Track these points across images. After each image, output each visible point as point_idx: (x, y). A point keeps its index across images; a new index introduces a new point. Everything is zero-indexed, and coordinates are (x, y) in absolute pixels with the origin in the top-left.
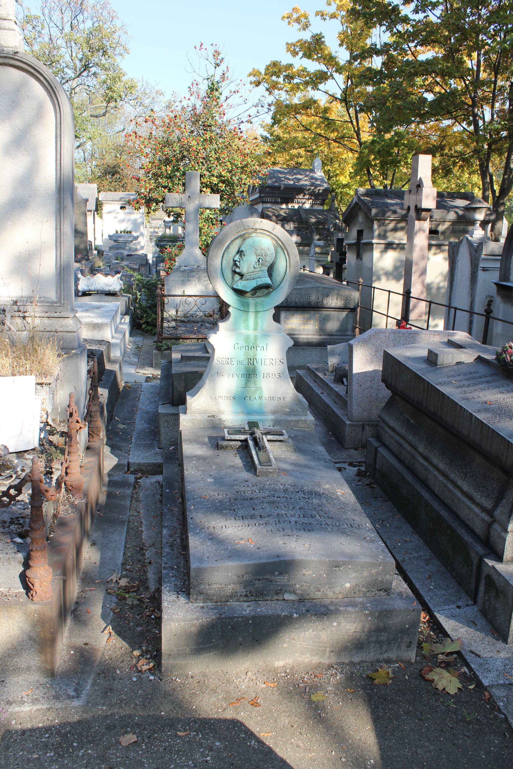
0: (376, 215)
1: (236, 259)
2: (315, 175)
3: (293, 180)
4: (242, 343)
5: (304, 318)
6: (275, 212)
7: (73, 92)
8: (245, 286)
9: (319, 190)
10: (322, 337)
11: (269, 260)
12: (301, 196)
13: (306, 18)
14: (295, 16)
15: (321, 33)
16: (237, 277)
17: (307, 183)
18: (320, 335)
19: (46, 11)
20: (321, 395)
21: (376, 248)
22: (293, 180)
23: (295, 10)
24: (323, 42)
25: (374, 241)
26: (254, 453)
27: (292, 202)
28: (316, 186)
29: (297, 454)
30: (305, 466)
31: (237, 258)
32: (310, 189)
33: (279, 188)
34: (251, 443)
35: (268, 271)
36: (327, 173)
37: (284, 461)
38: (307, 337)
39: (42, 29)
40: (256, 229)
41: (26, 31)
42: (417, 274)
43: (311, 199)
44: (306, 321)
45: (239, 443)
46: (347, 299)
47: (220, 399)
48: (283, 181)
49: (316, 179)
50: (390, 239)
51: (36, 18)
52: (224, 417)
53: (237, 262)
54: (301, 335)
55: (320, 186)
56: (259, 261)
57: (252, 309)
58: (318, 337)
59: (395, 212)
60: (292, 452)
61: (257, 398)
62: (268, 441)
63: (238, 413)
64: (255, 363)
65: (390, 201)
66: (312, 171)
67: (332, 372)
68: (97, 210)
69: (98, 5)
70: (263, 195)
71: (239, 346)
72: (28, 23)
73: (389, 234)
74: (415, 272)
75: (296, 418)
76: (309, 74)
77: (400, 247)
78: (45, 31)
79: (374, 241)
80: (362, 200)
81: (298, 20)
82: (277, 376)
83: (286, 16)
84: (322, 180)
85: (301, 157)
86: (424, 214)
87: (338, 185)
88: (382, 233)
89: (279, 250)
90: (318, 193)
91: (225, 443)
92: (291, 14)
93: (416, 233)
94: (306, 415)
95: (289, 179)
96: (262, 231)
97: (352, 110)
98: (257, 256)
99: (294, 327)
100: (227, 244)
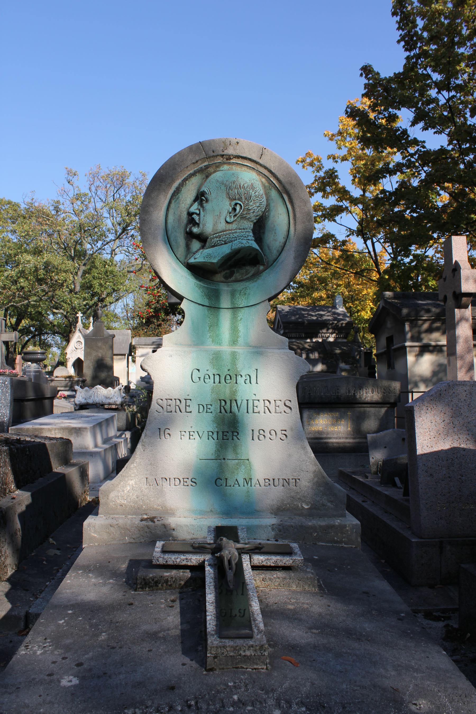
0: (408, 315)
1: (193, 209)
2: (337, 311)
3: (315, 316)
4: (207, 368)
5: (333, 418)
6: (300, 345)
7: (114, 253)
8: (209, 256)
9: (342, 324)
10: (357, 440)
11: (256, 208)
12: (324, 331)
13: (319, 161)
14: (308, 160)
15: (334, 168)
16: (196, 245)
17: (330, 318)
18: (354, 438)
19: (93, 189)
20: (363, 504)
21: (410, 352)
22: (315, 316)
23: (308, 154)
24: (336, 177)
25: (407, 344)
26: (210, 597)
27: (316, 337)
28: (339, 320)
29: (325, 601)
30: (349, 633)
31: (194, 208)
32: (333, 323)
33: (303, 323)
34: (209, 570)
35: (254, 231)
36: (349, 309)
37: (292, 616)
38: (337, 441)
39: (89, 202)
40: (229, 158)
41: (74, 204)
42: (464, 370)
43: (334, 333)
44: (336, 421)
45: (188, 574)
46: (387, 391)
47: (166, 484)
48: (306, 317)
49: (339, 314)
50: (425, 341)
51: (85, 195)
52: (172, 521)
53: (194, 216)
54: (330, 438)
55: (342, 320)
56: (234, 209)
57: (225, 302)
58: (351, 441)
59: (428, 311)
60: (314, 594)
61: (241, 481)
62: (254, 568)
63: (202, 513)
64: (235, 409)
65: (420, 302)
66: (334, 307)
67: (376, 473)
68: (130, 354)
69: (137, 181)
70: (287, 331)
71: (201, 375)
72: (78, 199)
73: (423, 335)
74: (461, 368)
75: (322, 523)
76: (325, 209)
77: (437, 349)
78: (91, 206)
79: (407, 344)
80: (389, 302)
81: (311, 164)
82: (280, 435)
83: (300, 160)
84: (344, 315)
85: (323, 300)
86: (464, 299)
87: (360, 320)
88: (416, 335)
89: (274, 193)
90: (342, 326)
91: (153, 574)
92: (305, 158)
93: (458, 323)
94: (344, 516)
95: (312, 316)
96: (240, 161)
97: (369, 242)
98: (231, 199)
99: (320, 428)
100: (176, 184)
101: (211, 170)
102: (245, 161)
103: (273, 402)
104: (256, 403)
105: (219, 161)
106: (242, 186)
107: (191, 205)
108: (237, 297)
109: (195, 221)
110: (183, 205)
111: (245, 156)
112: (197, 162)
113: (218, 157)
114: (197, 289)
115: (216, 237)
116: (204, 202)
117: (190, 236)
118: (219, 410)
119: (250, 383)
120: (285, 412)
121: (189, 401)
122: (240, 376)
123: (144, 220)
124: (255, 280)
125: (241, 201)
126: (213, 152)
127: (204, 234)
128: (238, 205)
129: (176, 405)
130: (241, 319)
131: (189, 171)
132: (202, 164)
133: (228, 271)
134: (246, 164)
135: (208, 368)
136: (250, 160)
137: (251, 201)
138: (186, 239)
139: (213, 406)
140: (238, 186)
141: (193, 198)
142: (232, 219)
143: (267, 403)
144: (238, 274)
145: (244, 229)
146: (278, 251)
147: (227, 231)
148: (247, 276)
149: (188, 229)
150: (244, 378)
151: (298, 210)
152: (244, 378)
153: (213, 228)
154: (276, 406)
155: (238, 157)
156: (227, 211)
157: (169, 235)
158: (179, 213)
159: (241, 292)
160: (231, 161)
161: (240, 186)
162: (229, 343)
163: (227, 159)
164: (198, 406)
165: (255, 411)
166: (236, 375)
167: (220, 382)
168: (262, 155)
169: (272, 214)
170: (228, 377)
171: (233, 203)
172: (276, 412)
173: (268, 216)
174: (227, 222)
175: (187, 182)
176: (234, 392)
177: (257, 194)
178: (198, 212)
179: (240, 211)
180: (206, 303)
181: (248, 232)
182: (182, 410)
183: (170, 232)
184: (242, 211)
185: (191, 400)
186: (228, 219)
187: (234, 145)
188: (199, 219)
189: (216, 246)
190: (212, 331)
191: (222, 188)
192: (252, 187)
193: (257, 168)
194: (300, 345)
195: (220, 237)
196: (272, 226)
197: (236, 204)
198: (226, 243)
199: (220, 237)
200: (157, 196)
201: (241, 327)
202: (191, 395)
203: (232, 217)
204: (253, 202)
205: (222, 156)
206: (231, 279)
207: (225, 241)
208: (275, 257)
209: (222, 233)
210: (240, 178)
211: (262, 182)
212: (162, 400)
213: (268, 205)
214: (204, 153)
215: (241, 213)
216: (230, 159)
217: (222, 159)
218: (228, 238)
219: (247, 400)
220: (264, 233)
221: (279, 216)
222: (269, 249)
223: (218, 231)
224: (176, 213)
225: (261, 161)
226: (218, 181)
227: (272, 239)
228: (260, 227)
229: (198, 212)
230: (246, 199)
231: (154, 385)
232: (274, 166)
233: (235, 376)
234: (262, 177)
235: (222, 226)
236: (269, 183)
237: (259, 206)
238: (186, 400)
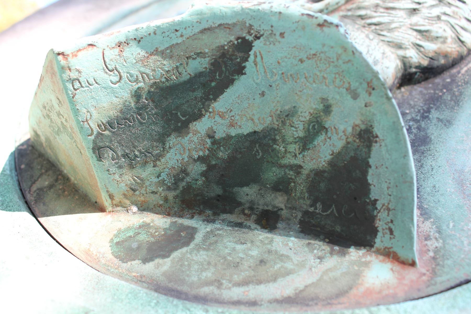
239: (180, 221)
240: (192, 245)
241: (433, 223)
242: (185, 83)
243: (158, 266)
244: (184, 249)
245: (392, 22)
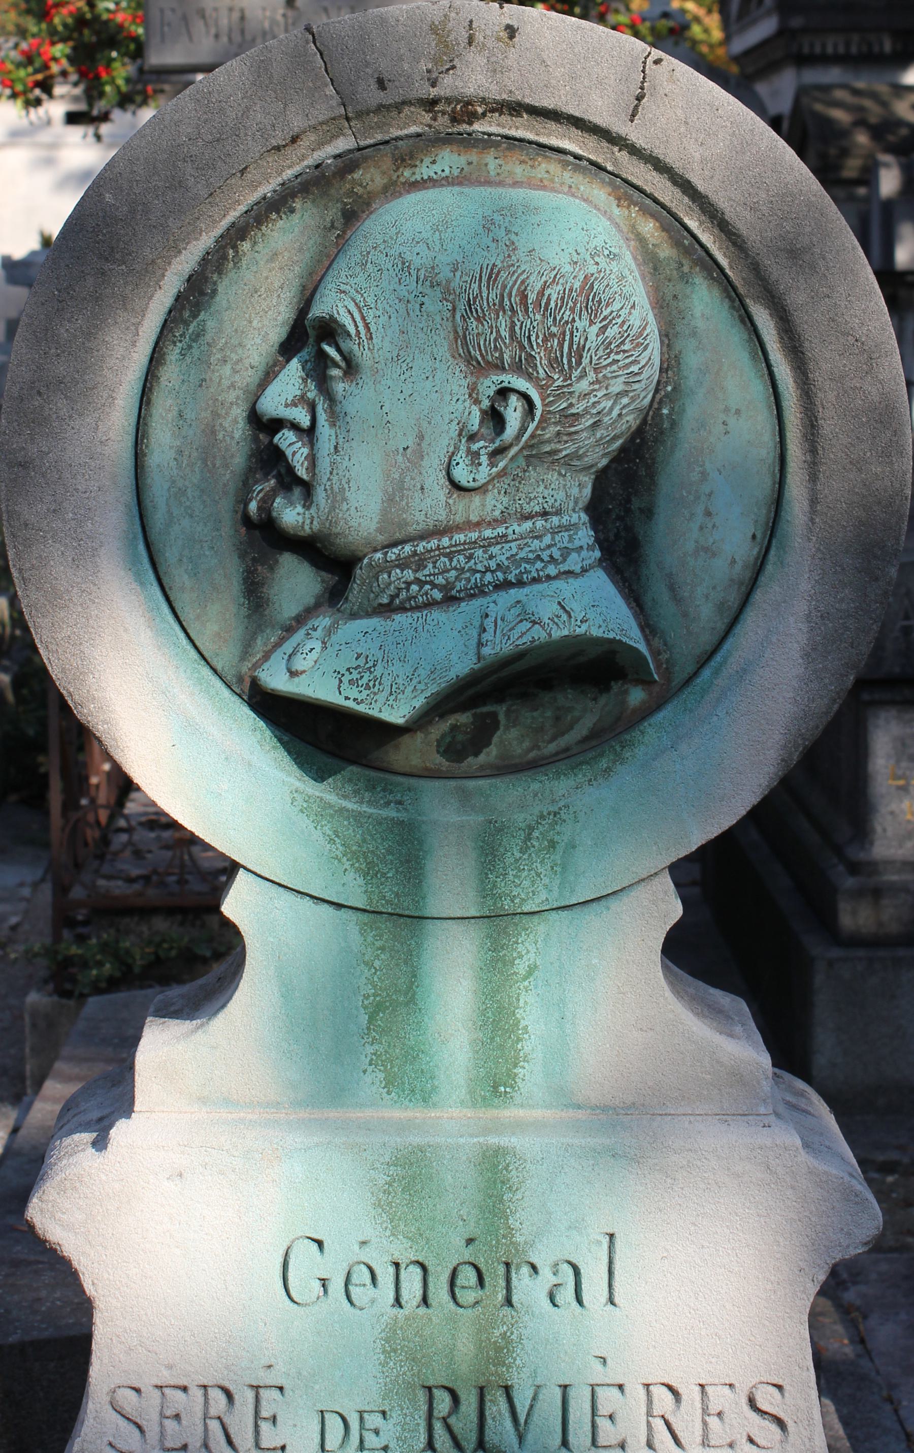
1: (274, 402)
6: (867, 103)
11: (608, 403)
31: (286, 393)
40: (466, 110)
53: (286, 439)
56: (495, 418)
57: (450, 886)
70: (796, 22)
71: (333, 1266)
89: (703, 302)
98: (479, 366)
101: (370, 177)
102: (552, 125)
103: (691, 1394)
104: (608, 1399)
105: (413, 129)
106: (532, 297)
107: (269, 376)
108: (509, 860)
109: (290, 470)
110: (227, 370)
111: (547, 102)
112: (294, 140)
113: (406, 110)
114: (305, 823)
115: (402, 564)
116: (335, 372)
117: (264, 539)
118: (423, 1438)
119: (579, 1300)
120: (751, 1440)
121: (276, 1394)
122: (525, 1270)
123: (24, 465)
124: (604, 763)
125: (529, 377)
126: (381, 84)
127: (340, 541)
128: (513, 399)
129: (206, 1417)
130: (532, 970)
131: (254, 186)
132: (321, 144)
133: (464, 718)
134: (554, 142)
135: (368, 1231)
136: (578, 123)
137: (584, 375)
138: (242, 556)
139: (395, 1416)
140: (516, 299)
141: (277, 333)
142: (484, 473)
143: (663, 1397)
144: (514, 733)
145: (545, 514)
146: (721, 607)
147: (458, 528)
148: (563, 742)
149: (253, 506)
150: (547, 1278)
151: (831, 396)
152: (547, 1278)
153: (384, 513)
154: (705, 1411)
155: (515, 108)
156: (454, 427)
157: (153, 536)
158: (207, 414)
159: (528, 838)
160: (477, 127)
161: (524, 297)
162: (471, 1092)
163: (454, 120)
164: (317, 1419)
165: (601, 1441)
166: (507, 1265)
167: (425, 1301)
168: (639, 98)
169: (692, 412)
170: (468, 1276)
171: (488, 386)
172: (705, 1443)
173: (674, 424)
174: (456, 486)
175: (246, 246)
176: (498, 1350)
177: (610, 332)
178: (302, 417)
179: (523, 429)
180: (353, 889)
181: (567, 528)
182: (236, 1440)
183: (158, 519)
184: (532, 427)
185: (281, 1389)
186: (462, 474)
187: (490, 43)
188: (312, 460)
189: (402, 609)
190: (384, 1032)
191: (429, 306)
192: (589, 299)
193: (615, 163)
194: (867, 103)
195: (420, 566)
196: (695, 476)
197: (504, 393)
198: (450, 600)
199: (419, 562)
200: (89, 335)
201: (532, 1013)
202: (280, 1367)
203: (484, 459)
204: (592, 376)
205: (430, 104)
206: (482, 758)
207: (446, 588)
208: (706, 639)
209: (433, 544)
210: (521, 253)
211: (641, 240)
212: (138, 1390)
213: (670, 365)
214: (330, 90)
215: (533, 436)
216: (472, 117)
217: (427, 117)
218: (462, 570)
219: (565, 1388)
220: (649, 513)
221: (732, 421)
222: (677, 599)
223: (412, 530)
224: (189, 415)
225: (635, 134)
226: (405, 266)
227: (690, 546)
228: (626, 500)
229: (305, 420)
230: (555, 362)
231: (98, 1318)
232: (703, 160)
233: (502, 1269)
234: (644, 210)
235: (431, 503)
236: (677, 244)
237: (624, 393)
238: (256, 1388)
239: (479, 710)
240: (502, 728)
241: (660, 638)
242: (883, 1228)
243: (488, 754)
244: (498, 733)
245: (579, 448)
